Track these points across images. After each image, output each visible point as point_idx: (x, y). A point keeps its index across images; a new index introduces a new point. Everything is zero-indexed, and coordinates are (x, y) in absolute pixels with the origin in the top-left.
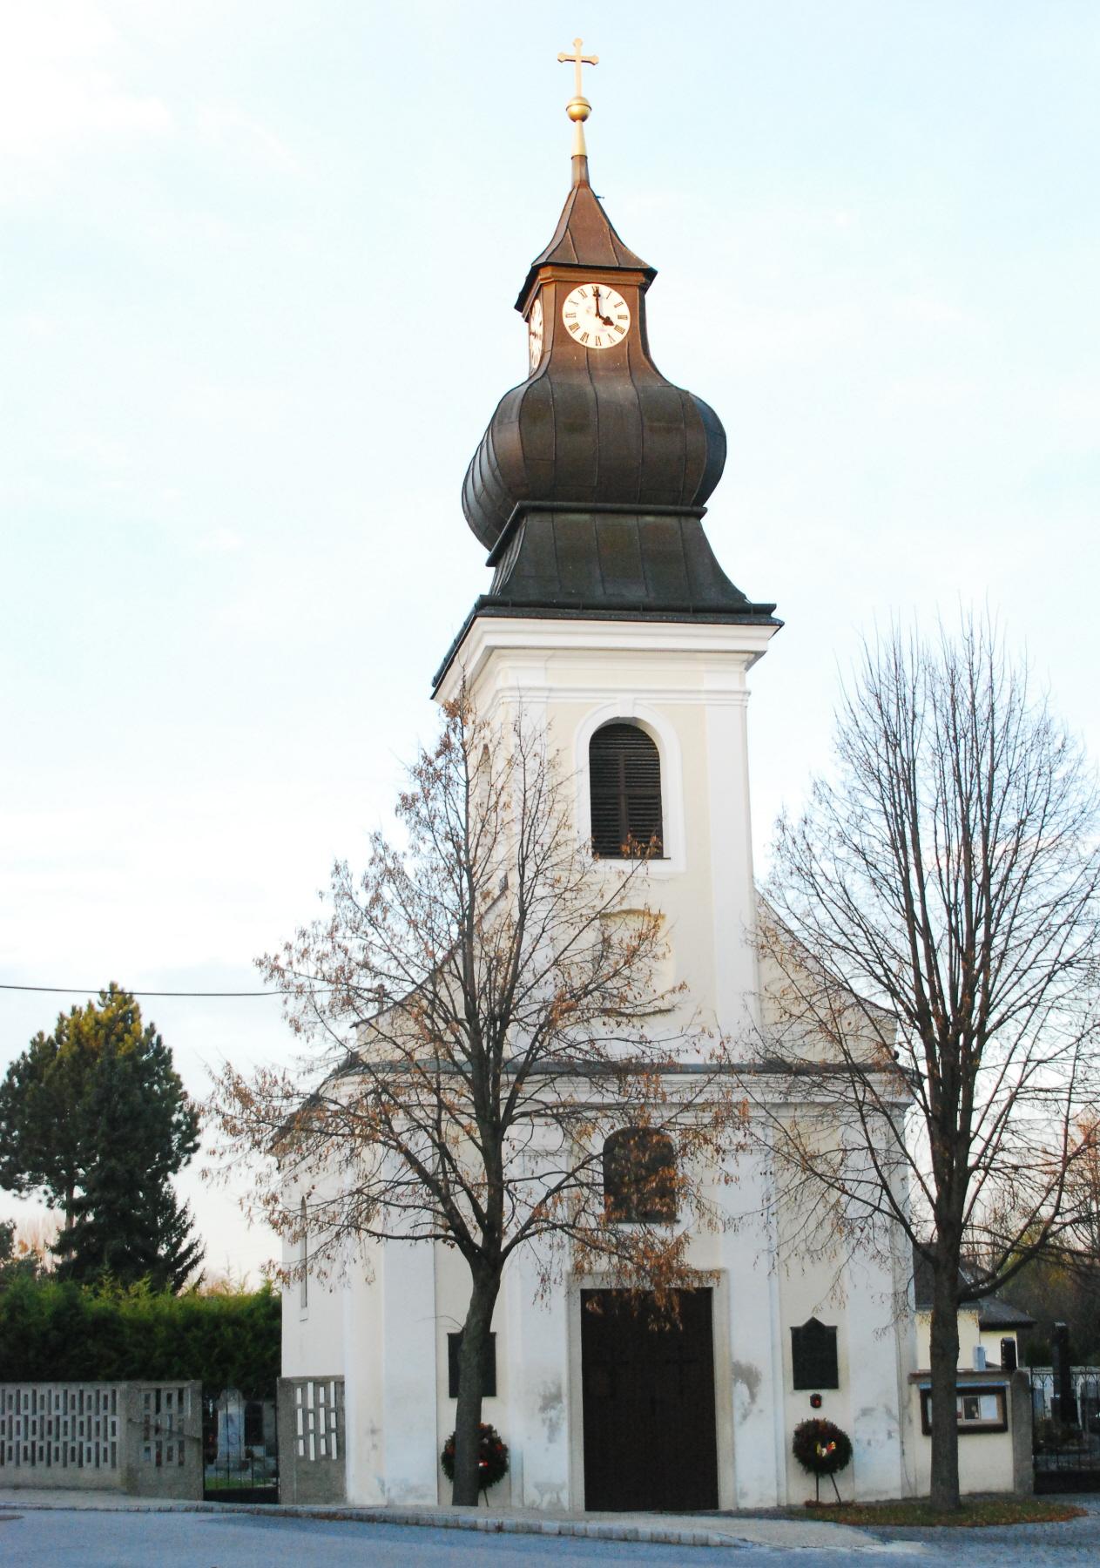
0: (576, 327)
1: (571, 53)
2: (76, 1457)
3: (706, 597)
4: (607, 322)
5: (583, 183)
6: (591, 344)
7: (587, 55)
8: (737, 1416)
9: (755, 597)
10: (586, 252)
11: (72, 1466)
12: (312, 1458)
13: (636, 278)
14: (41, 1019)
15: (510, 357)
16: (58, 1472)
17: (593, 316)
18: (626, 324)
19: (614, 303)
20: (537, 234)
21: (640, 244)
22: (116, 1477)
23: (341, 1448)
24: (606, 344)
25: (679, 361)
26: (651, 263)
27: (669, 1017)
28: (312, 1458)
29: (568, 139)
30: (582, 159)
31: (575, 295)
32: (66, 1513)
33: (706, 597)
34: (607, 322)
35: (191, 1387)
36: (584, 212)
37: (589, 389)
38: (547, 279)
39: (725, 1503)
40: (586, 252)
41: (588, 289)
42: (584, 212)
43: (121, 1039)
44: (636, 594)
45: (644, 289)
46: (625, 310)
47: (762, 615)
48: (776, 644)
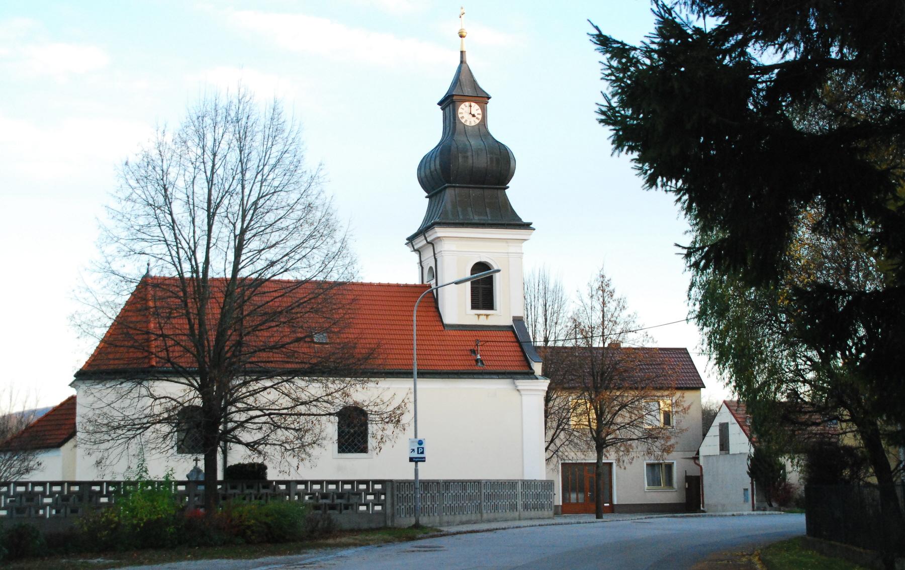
0: (463, 117)
3: (509, 220)
4: (474, 116)
6: (468, 124)
9: (525, 220)
10: (463, 91)
12: (66, 493)
13: (482, 98)
18: (480, 117)
19: (476, 108)
23: (432, 537)
24: (473, 124)
25: (499, 131)
28: (66, 493)
31: (463, 106)
32: (469, 535)
33: (509, 220)
34: (474, 116)
37: (467, 143)
38: (449, 103)
39: (699, 474)
40: (463, 91)
41: (467, 104)
43: (346, 441)
46: (480, 111)
47: (527, 226)
48: (533, 236)
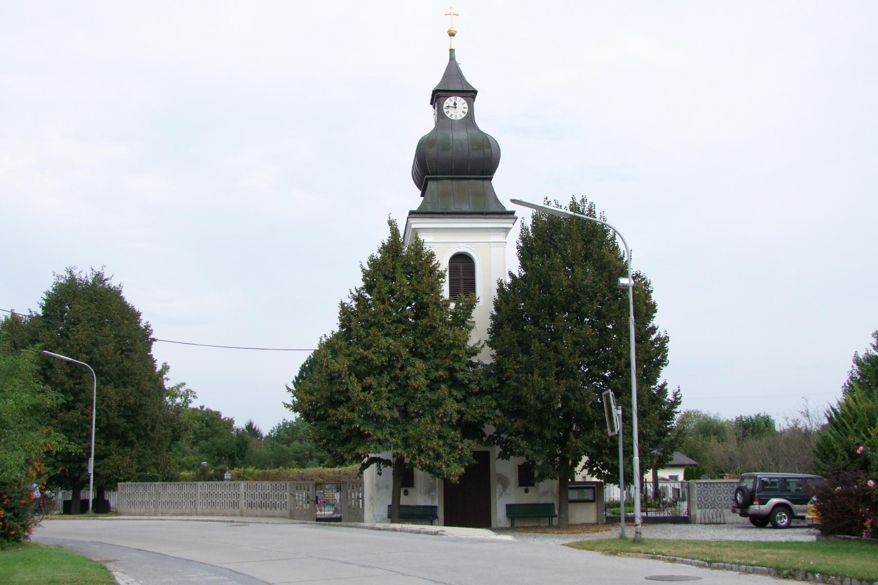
1: (449, 12)
2: (274, 506)
5: (452, 59)
6: (453, 118)
7: (454, 11)
8: (498, 495)
10: (453, 87)
11: (264, 509)
13: (470, 94)
14: (49, 285)
15: (425, 122)
16: (269, 511)
17: (456, 108)
19: (461, 102)
20: (435, 80)
21: (472, 79)
22: (287, 513)
25: (485, 123)
26: (476, 88)
27: (699, 581)
29: (447, 43)
30: (452, 51)
35: (455, 479)
36: (453, 71)
38: (438, 96)
40: (453, 87)
42: (453, 71)
44: (466, 208)
45: (474, 98)
